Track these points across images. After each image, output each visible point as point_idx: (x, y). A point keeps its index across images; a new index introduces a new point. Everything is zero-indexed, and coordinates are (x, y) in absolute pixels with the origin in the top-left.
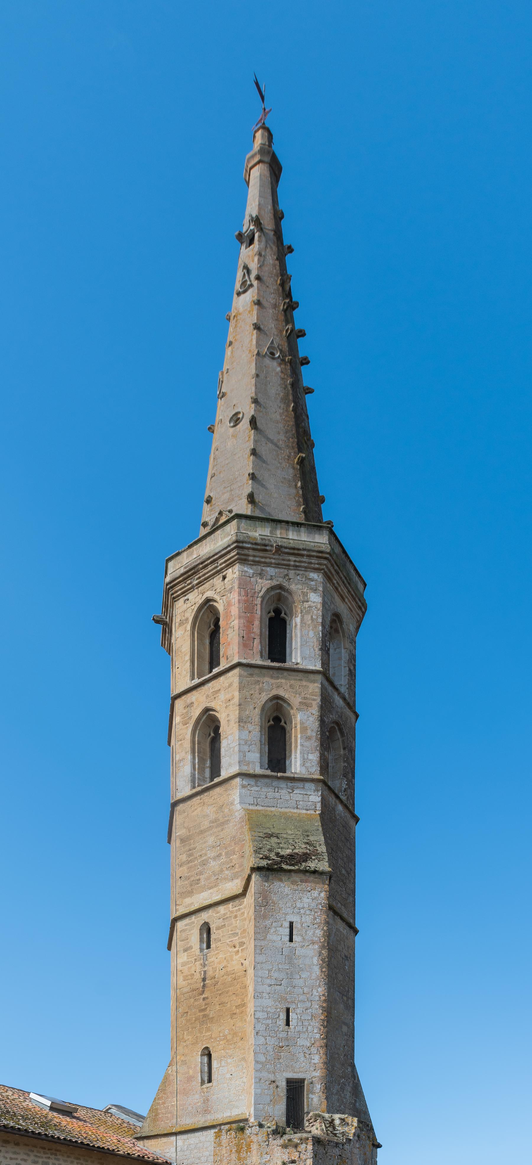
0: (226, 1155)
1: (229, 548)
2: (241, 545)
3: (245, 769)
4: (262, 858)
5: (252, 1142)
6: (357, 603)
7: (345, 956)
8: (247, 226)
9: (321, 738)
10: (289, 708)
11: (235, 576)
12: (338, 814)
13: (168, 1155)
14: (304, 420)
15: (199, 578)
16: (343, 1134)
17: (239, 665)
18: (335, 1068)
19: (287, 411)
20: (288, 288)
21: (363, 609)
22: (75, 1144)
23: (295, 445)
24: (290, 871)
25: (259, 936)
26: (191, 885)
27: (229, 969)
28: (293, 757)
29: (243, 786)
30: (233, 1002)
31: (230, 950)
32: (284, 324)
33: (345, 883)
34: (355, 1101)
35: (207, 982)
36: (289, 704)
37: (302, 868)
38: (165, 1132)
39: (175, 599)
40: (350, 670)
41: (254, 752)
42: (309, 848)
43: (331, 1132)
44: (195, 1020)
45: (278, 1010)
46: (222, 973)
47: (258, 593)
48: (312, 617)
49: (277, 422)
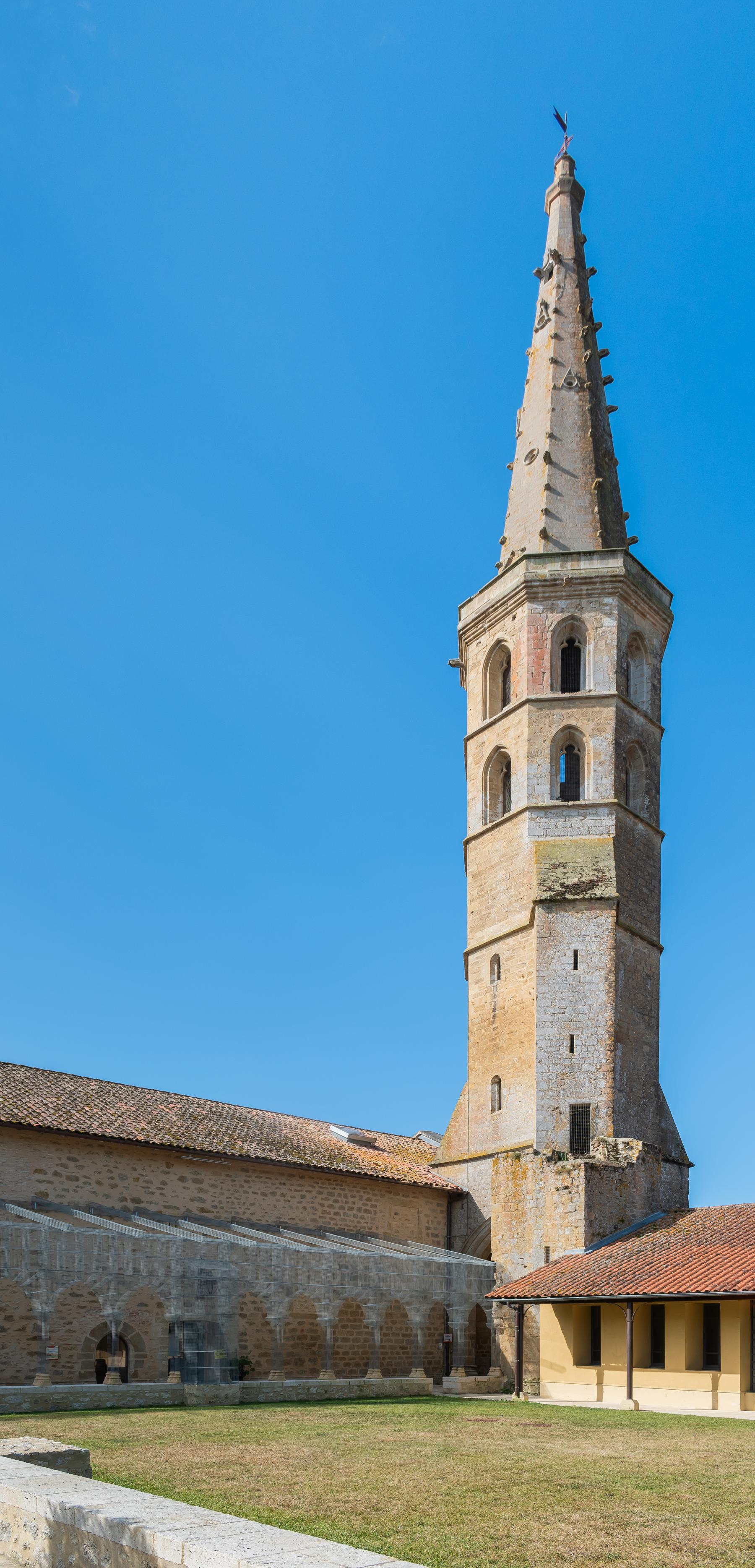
0: (503, 1182)
1: (518, 589)
2: (529, 584)
3: (534, 803)
4: (545, 891)
5: (527, 1169)
6: (660, 616)
7: (647, 975)
8: (547, 260)
9: (616, 761)
10: (581, 736)
11: (524, 615)
12: (638, 834)
13: (460, 1181)
14: (606, 440)
15: (490, 621)
16: (626, 1158)
17: (528, 701)
18: (634, 1090)
19: (584, 438)
20: (589, 312)
21: (669, 621)
22: (358, 1175)
23: (593, 470)
24: (574, 900)
25: (541, 967)
26: (482, 919)
27: (517, 999)
28: (586, 783)
29: (532, 819)
30: (521, 1031)
31: (519, 980)
32: (583, 350)
33: (646, 902)
34: (660, 1121)
35: (497, 1012)
36: (581, 732)
37: (586, 896)
38: (457, 1159)
39: (468, 644)
40: (653, 685)
41: (544, 784)
42: (597, 874)
43: (613, 1156)
44: (486, 1050)
45: (562, 1038)
46: (511, 1002)
47: (549, 628)
48: (606, 642)
49: (574, 451)
